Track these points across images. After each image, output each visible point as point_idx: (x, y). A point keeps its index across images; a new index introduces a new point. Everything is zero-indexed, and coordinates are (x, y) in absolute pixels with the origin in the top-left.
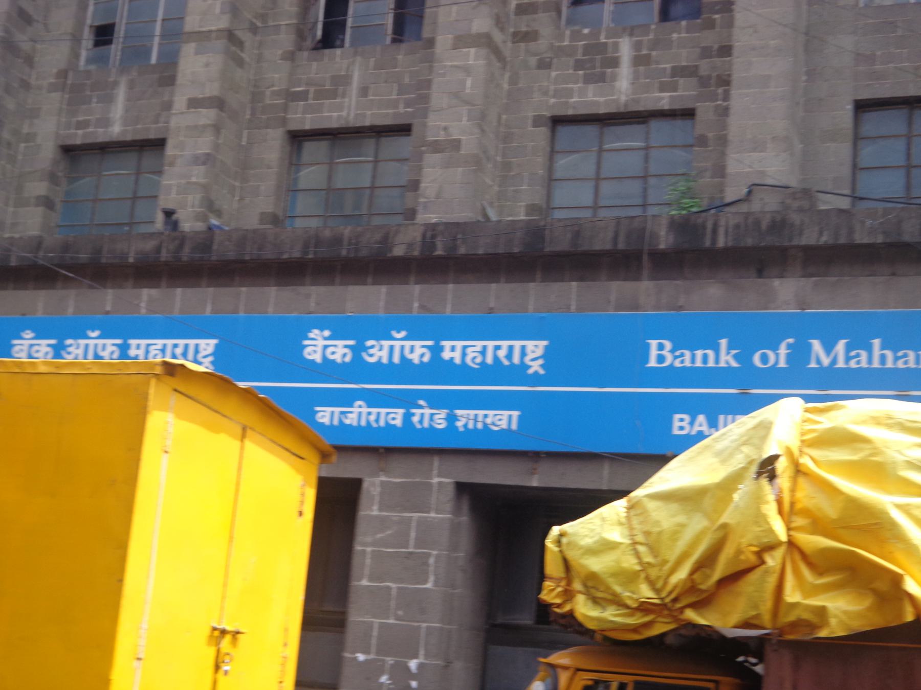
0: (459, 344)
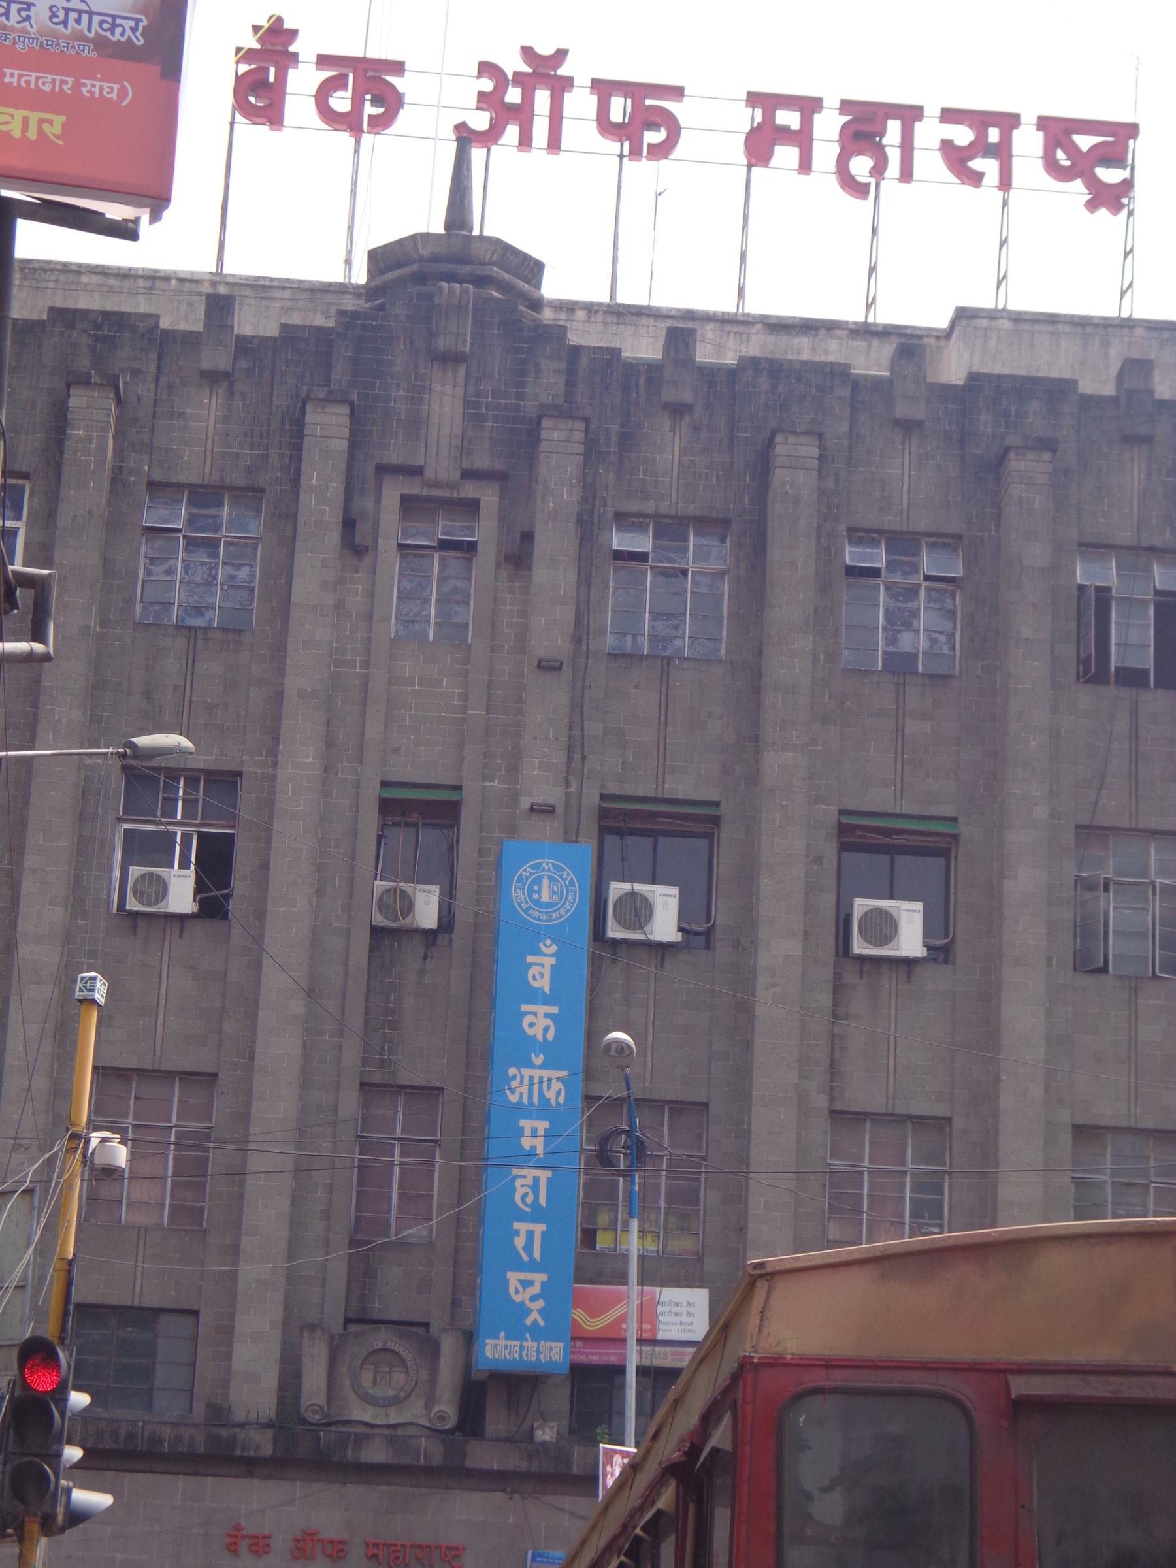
0: (16, 72)
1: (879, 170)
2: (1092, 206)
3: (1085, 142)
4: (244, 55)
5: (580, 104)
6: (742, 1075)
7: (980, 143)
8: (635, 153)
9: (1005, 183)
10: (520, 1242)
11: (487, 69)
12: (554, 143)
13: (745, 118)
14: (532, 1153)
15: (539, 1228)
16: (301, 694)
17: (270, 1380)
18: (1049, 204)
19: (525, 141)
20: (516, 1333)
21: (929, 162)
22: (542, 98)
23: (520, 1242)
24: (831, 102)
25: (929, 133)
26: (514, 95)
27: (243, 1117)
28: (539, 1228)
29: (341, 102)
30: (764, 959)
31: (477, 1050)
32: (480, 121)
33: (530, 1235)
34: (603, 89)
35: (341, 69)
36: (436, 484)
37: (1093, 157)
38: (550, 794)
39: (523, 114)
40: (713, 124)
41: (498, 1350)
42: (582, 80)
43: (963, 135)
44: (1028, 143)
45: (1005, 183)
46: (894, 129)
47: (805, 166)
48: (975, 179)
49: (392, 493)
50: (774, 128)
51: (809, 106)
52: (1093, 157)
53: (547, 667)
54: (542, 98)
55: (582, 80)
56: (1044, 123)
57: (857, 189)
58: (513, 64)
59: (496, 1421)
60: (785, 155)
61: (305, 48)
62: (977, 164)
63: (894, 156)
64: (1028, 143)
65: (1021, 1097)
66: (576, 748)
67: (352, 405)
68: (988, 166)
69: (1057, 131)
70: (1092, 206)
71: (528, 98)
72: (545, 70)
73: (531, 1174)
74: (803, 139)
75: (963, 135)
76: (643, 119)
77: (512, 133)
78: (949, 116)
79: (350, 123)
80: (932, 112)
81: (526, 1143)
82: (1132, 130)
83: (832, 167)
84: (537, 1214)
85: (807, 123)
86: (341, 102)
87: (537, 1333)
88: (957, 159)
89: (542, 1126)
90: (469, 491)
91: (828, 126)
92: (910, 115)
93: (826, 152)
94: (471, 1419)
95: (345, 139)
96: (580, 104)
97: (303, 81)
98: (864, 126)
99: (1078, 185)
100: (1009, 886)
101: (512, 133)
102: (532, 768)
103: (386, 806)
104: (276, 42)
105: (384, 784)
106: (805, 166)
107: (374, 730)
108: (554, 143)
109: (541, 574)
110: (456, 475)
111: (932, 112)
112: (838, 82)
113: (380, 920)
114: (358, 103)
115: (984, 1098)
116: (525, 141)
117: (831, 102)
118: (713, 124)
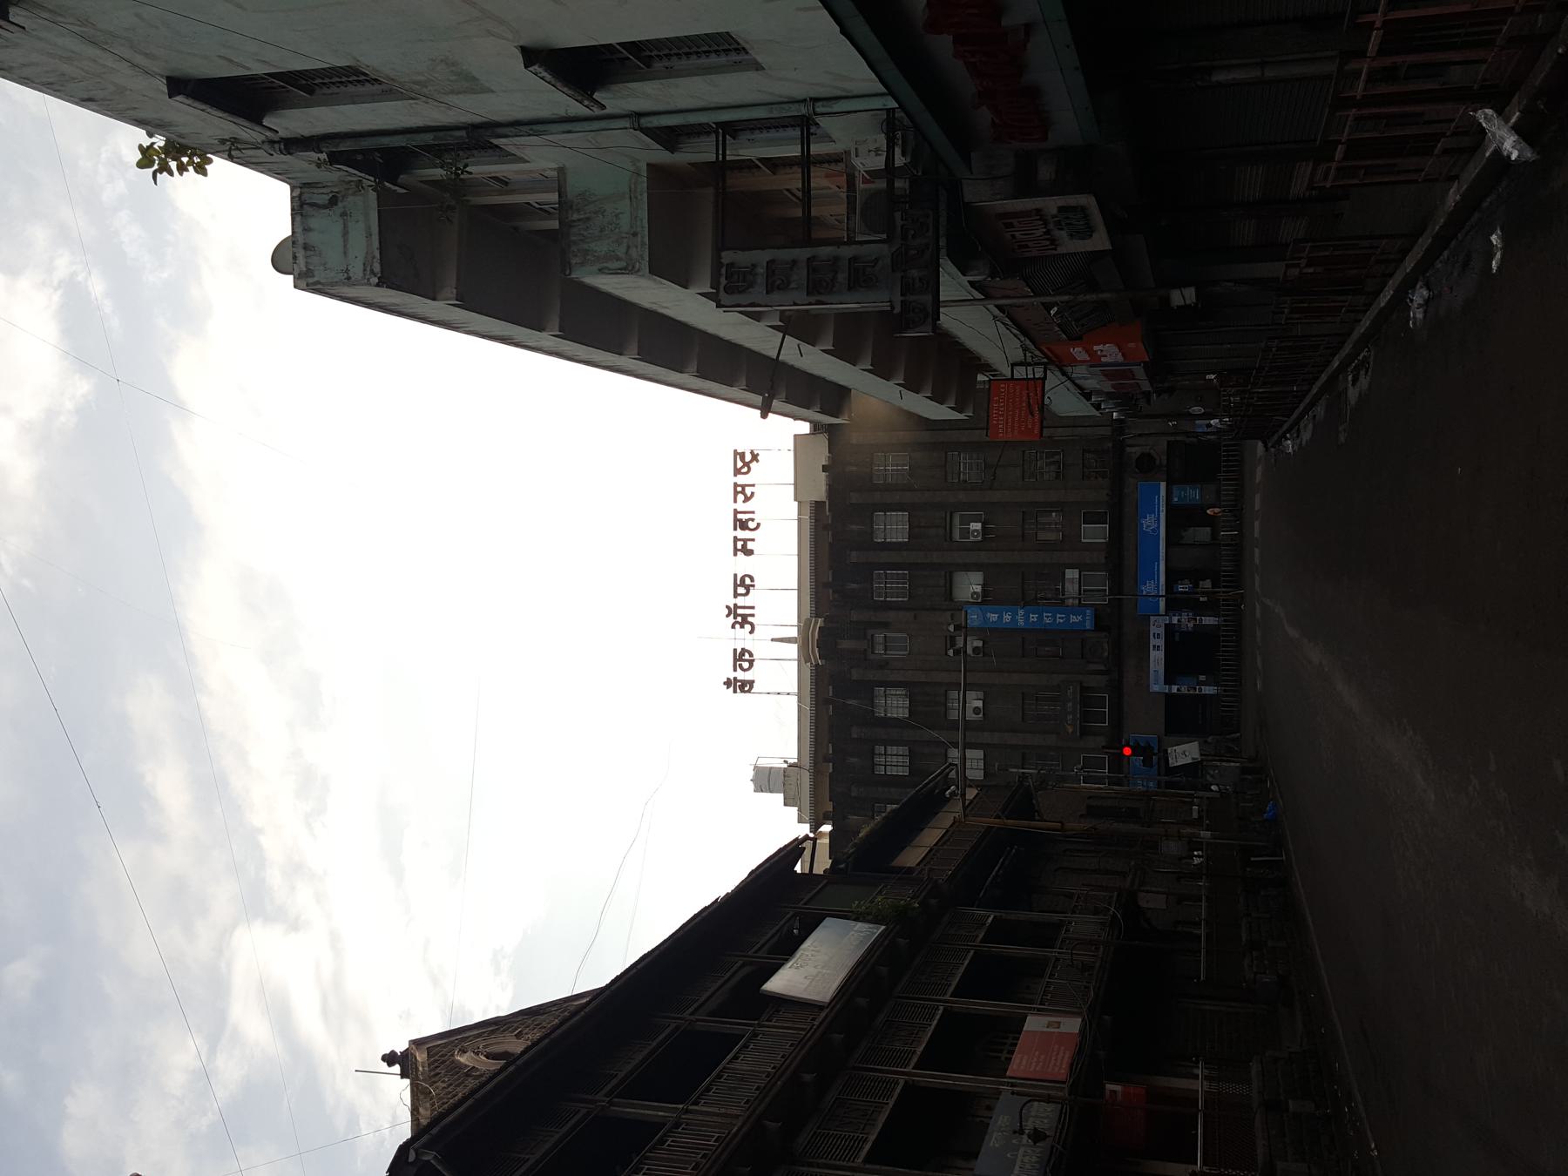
5: (740, 601)
18: (757, 473)
31: (1013, 631)
32: (748, 627)
34: (736, 595)
39: (744, 617)
40: (743, 565)
41: (1088, 625)
44: (741, 479)
52: (744, 462)
54: (740, 611)
58: (731, 620)
60: (750, 545)
64: (741, 479)
69: (737, 472)
72: (732, 611)
76: (743, 584)
79: (751, 662)
86: (746, 665)
91: (742, 534)
96: (740, 601)
97: (741, 675)
118: (743, 565)
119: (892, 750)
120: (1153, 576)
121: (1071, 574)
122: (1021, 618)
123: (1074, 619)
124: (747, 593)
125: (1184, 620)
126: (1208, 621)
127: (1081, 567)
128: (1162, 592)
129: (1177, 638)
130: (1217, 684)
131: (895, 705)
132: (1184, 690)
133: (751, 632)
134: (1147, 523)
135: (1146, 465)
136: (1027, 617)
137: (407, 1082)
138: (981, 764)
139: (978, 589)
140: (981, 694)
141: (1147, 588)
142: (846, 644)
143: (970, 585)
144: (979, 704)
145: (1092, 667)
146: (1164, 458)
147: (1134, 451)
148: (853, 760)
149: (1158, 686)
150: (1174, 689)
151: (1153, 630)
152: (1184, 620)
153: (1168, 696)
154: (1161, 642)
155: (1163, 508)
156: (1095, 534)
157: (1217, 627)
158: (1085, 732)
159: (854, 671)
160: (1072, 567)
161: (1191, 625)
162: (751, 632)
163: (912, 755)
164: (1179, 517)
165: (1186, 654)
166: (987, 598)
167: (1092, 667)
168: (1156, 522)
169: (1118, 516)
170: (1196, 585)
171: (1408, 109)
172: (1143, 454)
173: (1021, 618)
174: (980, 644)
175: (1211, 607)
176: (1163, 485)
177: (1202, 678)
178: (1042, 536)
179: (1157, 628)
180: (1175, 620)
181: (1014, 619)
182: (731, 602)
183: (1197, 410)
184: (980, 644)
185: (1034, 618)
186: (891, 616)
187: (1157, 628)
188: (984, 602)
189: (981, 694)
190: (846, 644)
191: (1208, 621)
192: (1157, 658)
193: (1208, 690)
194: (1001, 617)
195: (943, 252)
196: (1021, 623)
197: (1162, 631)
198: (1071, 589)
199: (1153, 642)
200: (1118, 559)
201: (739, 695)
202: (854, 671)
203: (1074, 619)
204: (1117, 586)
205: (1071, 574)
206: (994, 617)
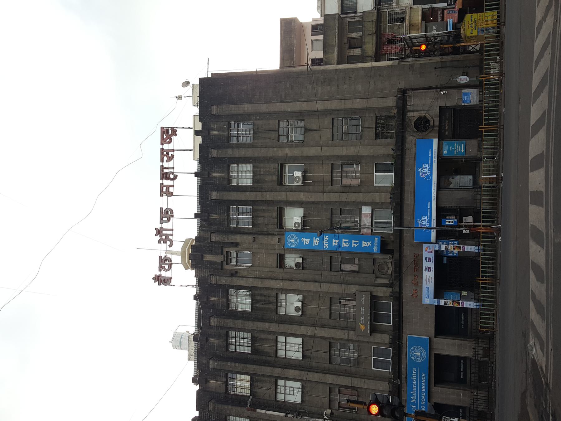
1: (173, 173)
2: (176, 135)
3: (165, 137)
4: (159, 284)
5: (164, 226)
6: (325, 203)
7: (166, 155)
8: (172, 216)
9: (173, 151)
10: (356, 245)
11: (159, 242)
12: (172, 230)
13: (165, 197)
14: (338, 243)
15: (353, 241)
16: (261, 284)
17: (385, 289)
18: (178, 142)
19: (172, 235)
20: (373, 246)
21: (171, 164)
22: (164, 232)
23: (356, 245)
24: (161, 182)
25: (165, 164)
26: (164, 237)
27: (337, 293)
28: (353, 241)
29: (167, 267)
30: (304, 200)
31: (321, 252)
32: (168, 243)
33: (354, 243)
34: (161, 221)
35: (161, 268)
36: (224, 260)
37: (168, 134)
38: (277, 238)
39: (167, 236)
40: (166, 202)
41: (376, 249)
42: (160, 225)
43: (165, 158)
44: (166, 147)
45: (173, 151)
46: (165, 171)
47: (173, 186)
48: (173, 156)
49: (226, 267)
50: (166, 192)
51: (162, 186)
52: (168, 134)
53: (254, 240)
54: (164, 232)
55: (160, 225)
56: (162, 144)
57: (176, 177)
58: (158, 237)
59: (390, 247)
60: (171, 189)
61: (158, 273)
62: (170, 156)
63: (170, 170)
64: (166, 147)
65: (327, 152)
66: (269, 234)
67: (211, 275)
68: (171, 153)
69: (163, 142)
70: (176, 135)
71: (164, 235)
72: (159, 232)
73: (343, 243)
74: (168, 187)
75: (165, 158)
76: (166, 214)
77: (170, 237)
78: (162, 161)
79: (170, 266)
80: (161, 164)
81: (337, 244)
82: (162, 128)
83: (172, 181)
84: (350, 242)
85: (165, 186)
86: (167, 267)
87: (373, 243)
88: (170, 158)
89: (334, 241)
90: (225, 253)
91: (165, 182)
92: (162, 168)
93: (170, 183)
94: (390, 252)
95: (173, 266)
96: (164, 226)
97: (163, 274)
98: (165, 176)
99: (172, 138)
100: (289, 155)
101: (170, 237)
102: (272, 242)
103: (281, 267)
104: (157, 279)
105: (277, 267)
106: (173, 186)
107: (267, 269)
108: (172, 230)
109: (238, 241)
110: (222, 256)
111: (161, 164)
112: (157, 181)
113: (301, 268)
114: (166, 264)
115: (328, 158)
116: (172, 235)
117: (161, 182)
118: (166, 202)
119: (241, 334)
120: (426, 212)
121: (366, 210)
122: (327, 242)
123: (365, 244)
124: (169, 220)
125: (450, 248)
126: (471, 249)
127: (374, 205)
128: (434, 225)
129: (445, 261)
130: (477, 300)
131: (243, 302)
132: (450, 303)
133: (170, 246)
134: (423, 171)
135: (422, 125)
136: (330, 242)
137: (197, 387)
138: (301, 350)
139: (299, 220)
140: (301, 297)
141: (422, 222)
142: (209, 258)
143: (294, 216)
144: (299, 304)
145: (379, 281)
146: (437, 120)
147: (413, 115)
148: (213, 340)
149: (428, 299)
150: (442, 302)
151: (425, 255)
152: (450, 248)
153: (438, 307)
154: (432, 265)
155: (435, 160)
156: (385, 180)
157: (477, 254)
158: (374, 330)
159: (213, 278)
160: (366, 204)
161: (456, 251)
162: (170, 246)
163: (253, 339)
164: (447, 167)
165: (450, 274)
166: (305, 227)
167: (379, 281)
168: (429, 171)
169: (400, 165)
170: (460, 220)
171: (462, 366)
172: (420, 118)
173: (327, 242)
174: (300, 260)
175: (473, 237)
176: (435, 141)
177: (465, 293)
178: (346, 182)
179: (428, 254)
180: (443, 247)
181: (321, 243)
182: (158, 226)
183: (463, 79)
184: (300, 260)
185: (335, 243)
186: (238, 238)
187: (428, 254)
188: (303, 230)
189: (301, 297)
190: (209, 258)
191: (471, 249)
192: (428, 277)
193: (470, 304)
194: (311, 242)
195: (544, 232)
196: (326, 246)
197: (432, 256)
198: (366, 221)
199: (425, 264)
200: (398, 200)
201: (162, 286)
202: (213, 278)
203: (365, 244)
204: (399, 219)
205: (366, 210)
206: (306, 241)
